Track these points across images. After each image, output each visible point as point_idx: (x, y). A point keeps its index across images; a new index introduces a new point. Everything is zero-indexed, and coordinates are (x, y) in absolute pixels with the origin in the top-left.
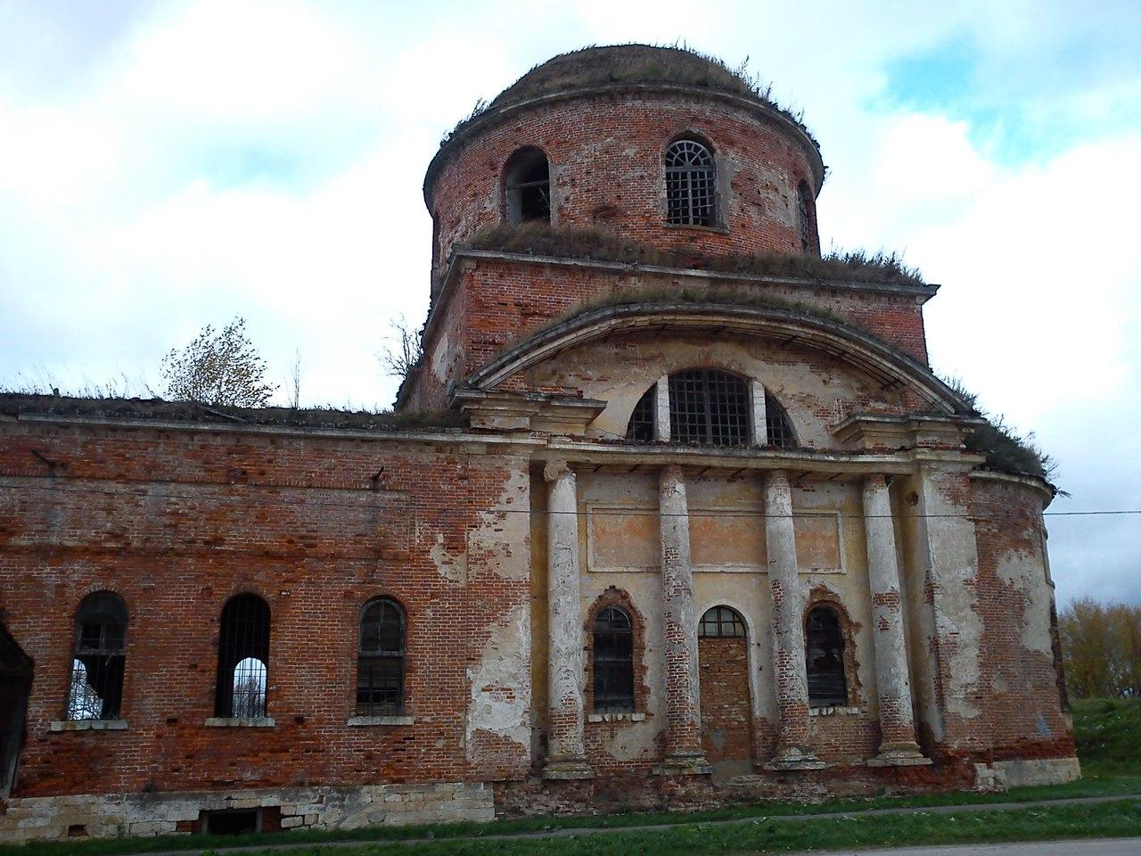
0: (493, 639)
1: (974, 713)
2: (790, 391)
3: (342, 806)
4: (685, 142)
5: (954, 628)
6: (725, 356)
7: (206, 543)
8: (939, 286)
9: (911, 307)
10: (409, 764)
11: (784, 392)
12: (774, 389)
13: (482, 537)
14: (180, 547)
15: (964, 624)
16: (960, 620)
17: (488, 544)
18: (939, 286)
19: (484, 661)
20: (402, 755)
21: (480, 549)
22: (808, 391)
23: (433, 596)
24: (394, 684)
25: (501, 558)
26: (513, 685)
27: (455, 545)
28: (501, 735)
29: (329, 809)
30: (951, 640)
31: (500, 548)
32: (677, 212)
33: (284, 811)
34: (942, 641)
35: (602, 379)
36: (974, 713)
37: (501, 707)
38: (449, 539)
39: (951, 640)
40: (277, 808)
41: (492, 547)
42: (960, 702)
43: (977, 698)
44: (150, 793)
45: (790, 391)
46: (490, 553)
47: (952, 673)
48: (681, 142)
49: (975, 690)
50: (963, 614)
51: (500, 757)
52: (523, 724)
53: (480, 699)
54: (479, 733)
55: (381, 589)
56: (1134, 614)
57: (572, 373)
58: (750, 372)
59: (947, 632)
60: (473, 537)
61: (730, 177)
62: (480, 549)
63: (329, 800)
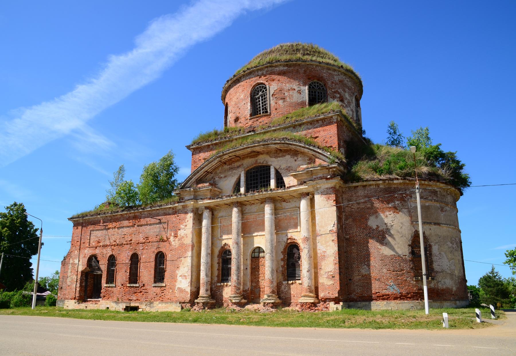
0: (182, 262)
1: (331, 282)
2: (282, 167)
3: (150, 307)
4: (258, 86)
5: (324, 250)
6: (262, 159)
7: (129, 241)
8: (69, 219)
9: (332, 121)
10: (164, 296)
11: (281, 168)
12: (277, 167)
13: (181, 233)
14: (125, 243)
15: (329, 248)
16: (327, 246)
17: (182, 235)
18: (69, 219)
19: (180, 268)
20: (163, 294)
21: (180, 236)
22: (289, 165)
23: (171, 250)
24: (369, 273)
25: (185, 238)
26: (186, 275)
27: (176, 236)
28: (183, 289)
29: (147, 307)
30: (323, 255)
31: (185, 235)
32: (255, 112)
33: (139, 307)
34: (319, 255)
35: (225, 177)
36: (331, 282)
37: (183, 281)
38: (175, 234)
39: (323, 255)
40: (138, 306)
41: (183, 235)
42: (325, 278)
43: (332, 277)
44: (117, 302)
45: (282, 167)
46: (183, 237)
47: (323, 267)
48: (257, 87)
49: (332, 274)
50: (328, 244)
51: (182, 295)
52: (188, 286)
53: (179, 279)
54: (179, 288)
55: (161, 250)
56: (31, 268)
57: (217, 177)
58: (269, 163)
59: (322, 251)
60: (179, 233)
61: (272, 93)
62: (180, 236)
63: (148, 305)
